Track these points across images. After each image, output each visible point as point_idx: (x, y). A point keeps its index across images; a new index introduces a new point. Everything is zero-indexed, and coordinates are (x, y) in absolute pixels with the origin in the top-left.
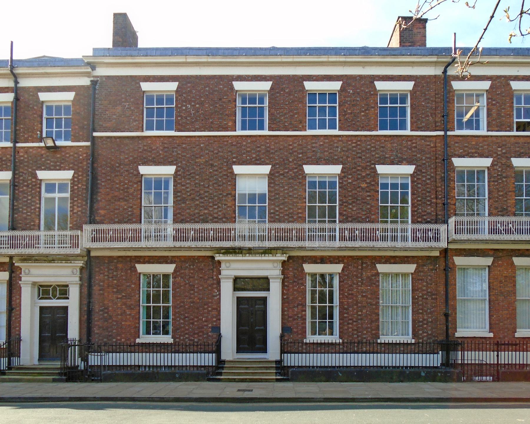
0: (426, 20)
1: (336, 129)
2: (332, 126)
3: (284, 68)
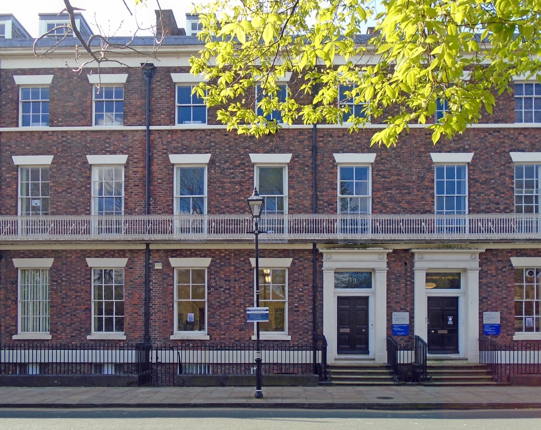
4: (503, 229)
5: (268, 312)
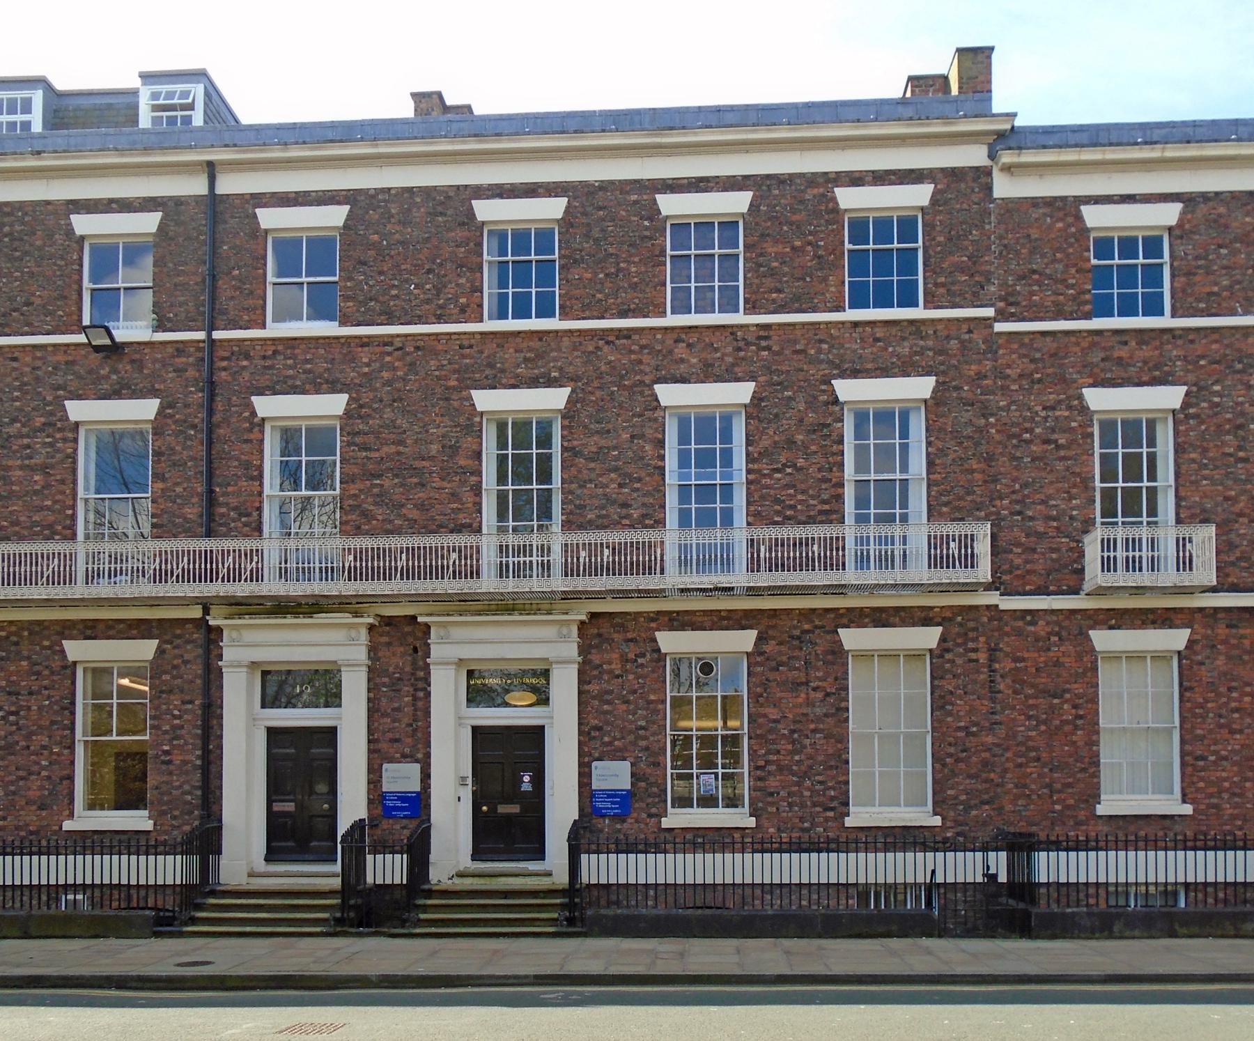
0: (992, 49)
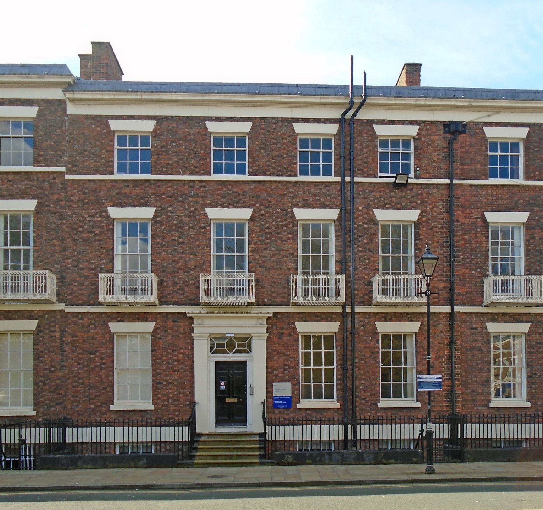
1: (331, 175)
2: (241, 171)
3: (256, 108)
4: (15, 287)
5: (441, 380)
